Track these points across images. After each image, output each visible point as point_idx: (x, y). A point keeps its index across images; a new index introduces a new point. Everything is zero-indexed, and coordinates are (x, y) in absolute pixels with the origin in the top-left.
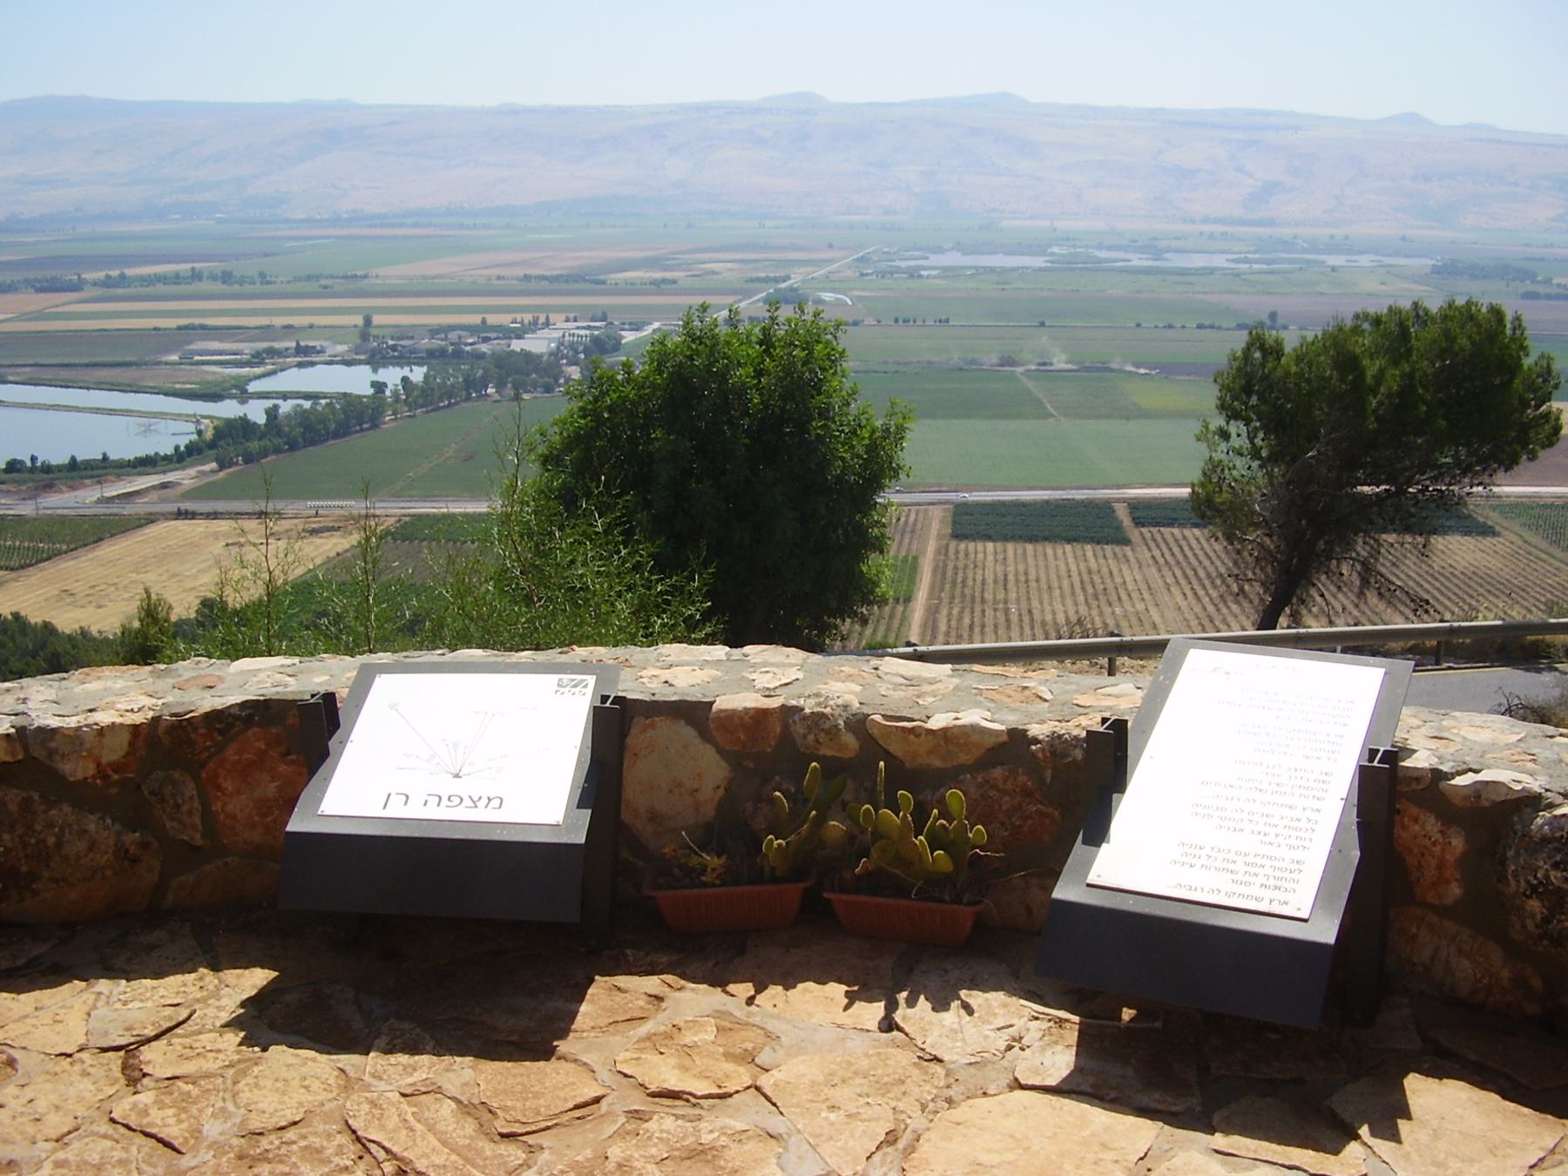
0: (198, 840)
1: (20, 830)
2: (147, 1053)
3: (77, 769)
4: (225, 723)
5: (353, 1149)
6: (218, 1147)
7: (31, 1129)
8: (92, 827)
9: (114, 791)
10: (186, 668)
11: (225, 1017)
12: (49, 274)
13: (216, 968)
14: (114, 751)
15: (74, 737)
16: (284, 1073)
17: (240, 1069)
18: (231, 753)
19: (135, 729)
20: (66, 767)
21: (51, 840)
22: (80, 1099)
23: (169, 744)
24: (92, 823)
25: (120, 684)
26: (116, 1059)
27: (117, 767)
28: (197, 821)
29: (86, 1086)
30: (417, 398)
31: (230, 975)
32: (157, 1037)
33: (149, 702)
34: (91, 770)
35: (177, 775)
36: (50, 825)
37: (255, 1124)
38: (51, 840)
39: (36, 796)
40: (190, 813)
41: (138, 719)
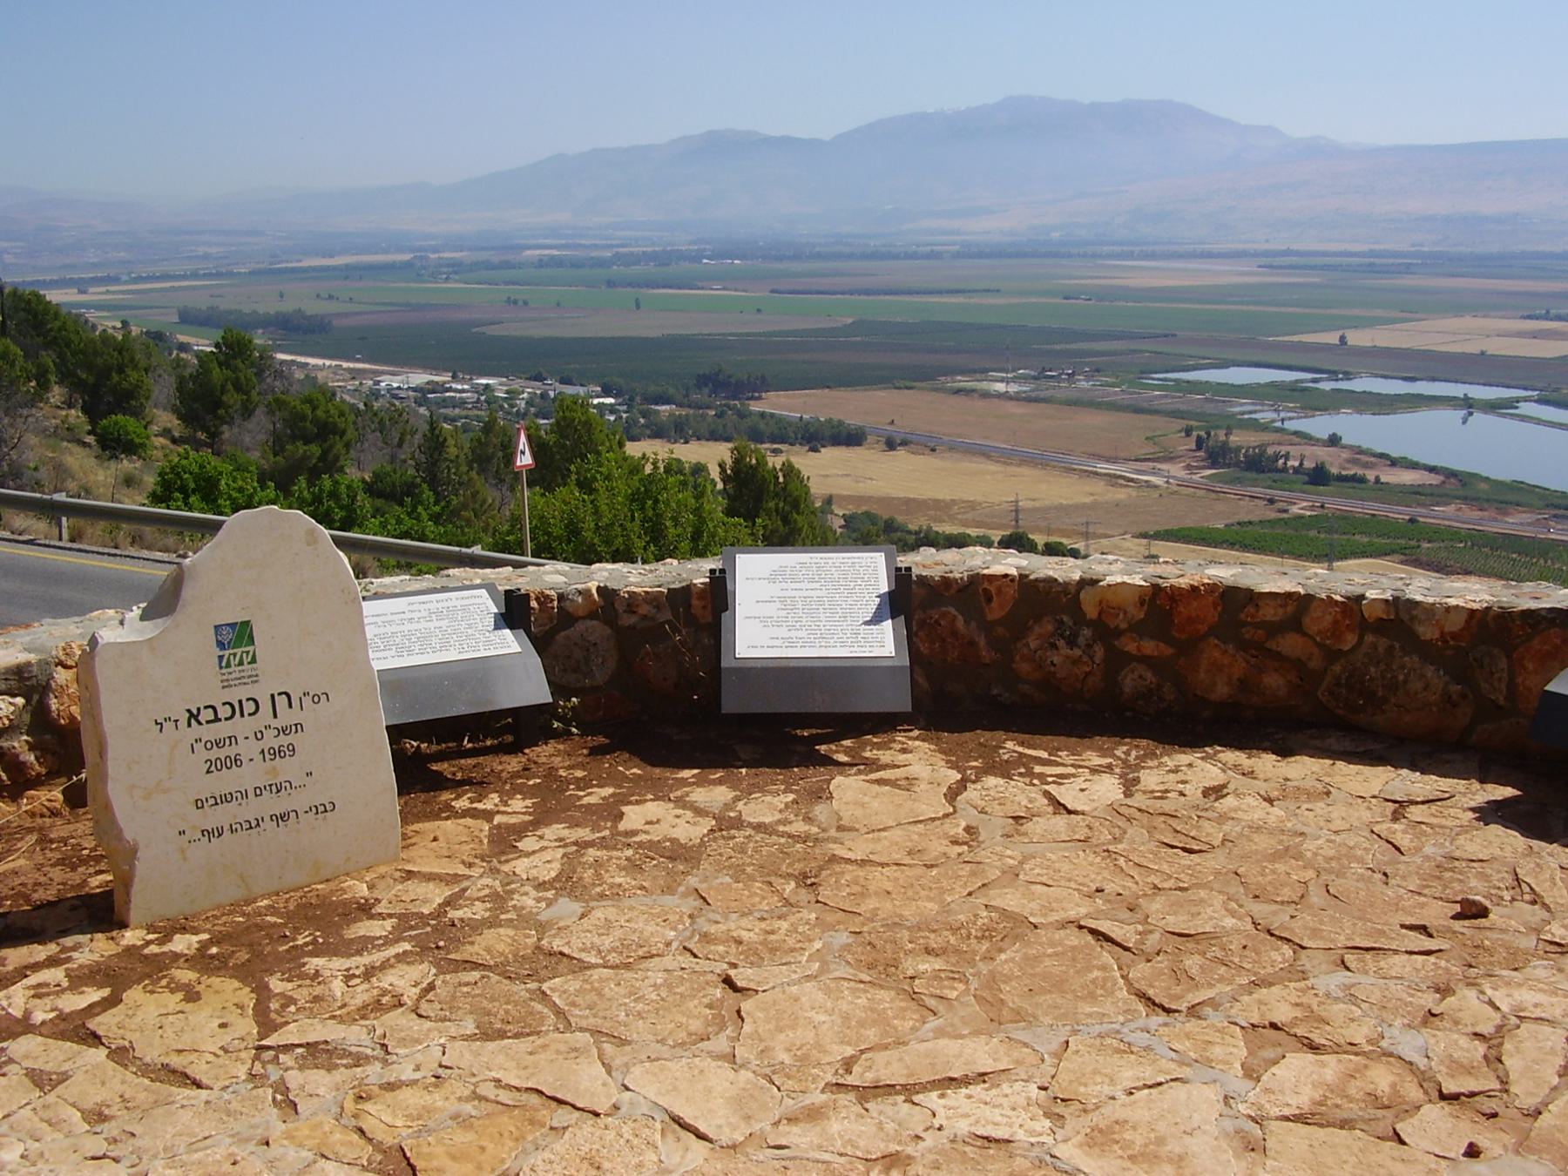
0: (1501, 701)
1: (1382, 667)
2: (1412, 808)
3: (1427, 632)
4: (1531, 617)
5: (1510, 881)
6: (1427, 858)
7: (1322, 824)
8: (1429, 674)
9: (1449, 652)
10: (1528, 586)
11: (1473, 804)
13: (1482, 782)
14: (1455, 624)
15: (1430, 609)
16: (1492, 838)
17: (1464, 829)
18: (1536, 642)
19: (1473, 611)
20: (1420, 629)
21: (1401, 678)
22: (1359, 818)
23: (1492, 627)
24: (1430, 671)
25: (1477, 586)
26: (1391, 806)
27: (1454, 636)
28: (1503, 686)
29: (1368, 814)
30: (952, 371)
31: (1489, 787)
32: (1423, 803)
33: (1488, 598)
34: (1436, 635)
35: (1496, 651)
36: (1403, 667)
37: (1457, 854)
38: (1401, 678)
39: (1397, 646)
40: (1500, 680)
41: (1475, 606)
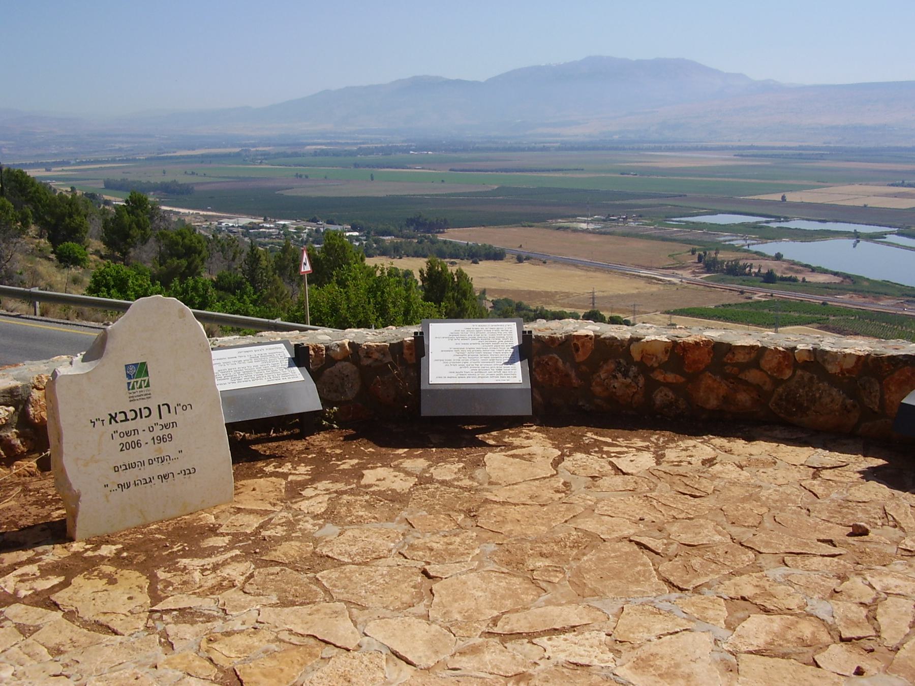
0: (876, 409)
1: (807, 389)
2: (824, 472)
3: (833, 369)
4: (893, 360)
5: (881, 514)
6: (833, 501)
7: (772, 481)
8: (834, 393)
9: (845, 381)
10: (892, 342)
11: (860, 469)
12: (671, 145)
13: (865, 456)
14: (849, 364)
15: (834, 355)
16: (871, 489)
17: (854, 484)
18: (896, 375)
19: (859, 357)
20: (829, 367)
21: (818, 395)
22: (793, 477)
23: (871, 366)
24: (834, 392)
25: (862, 342)
26: (812, 470)
27: (849, 371)
28: (877, 400)
29: (798, 475)
31: (869, 459)
32: (830, 468)
33: (868, 349)
34: (838, 371)
35: (873, 380)
36: (819, 389)
37: (850, 498)
38: (818, 395)
39: (815, 377)
40: (875, 396)
41: (861, 354)
